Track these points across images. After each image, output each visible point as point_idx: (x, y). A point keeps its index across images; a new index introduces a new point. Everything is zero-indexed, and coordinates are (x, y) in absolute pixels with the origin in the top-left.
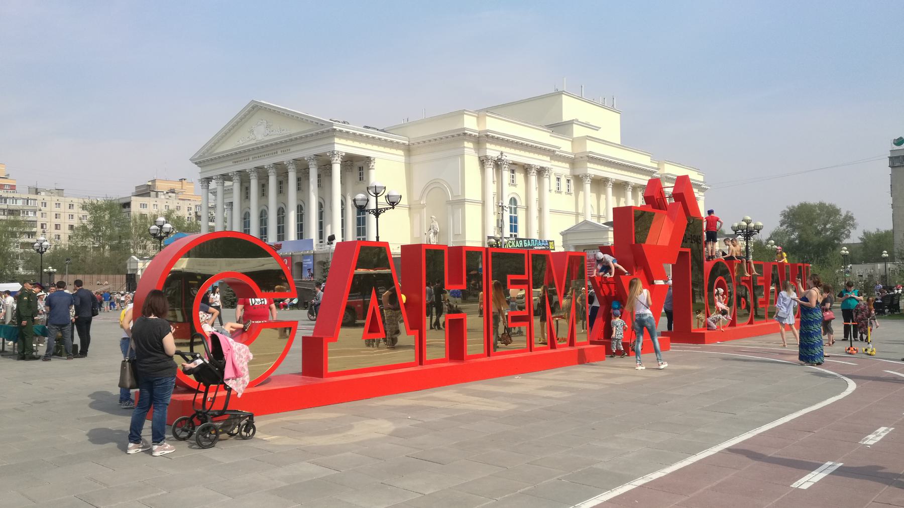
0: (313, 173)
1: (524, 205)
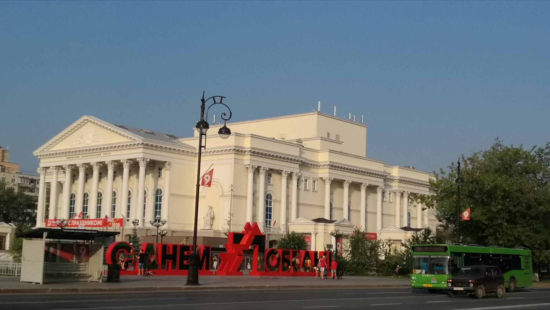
0: (96, 173)
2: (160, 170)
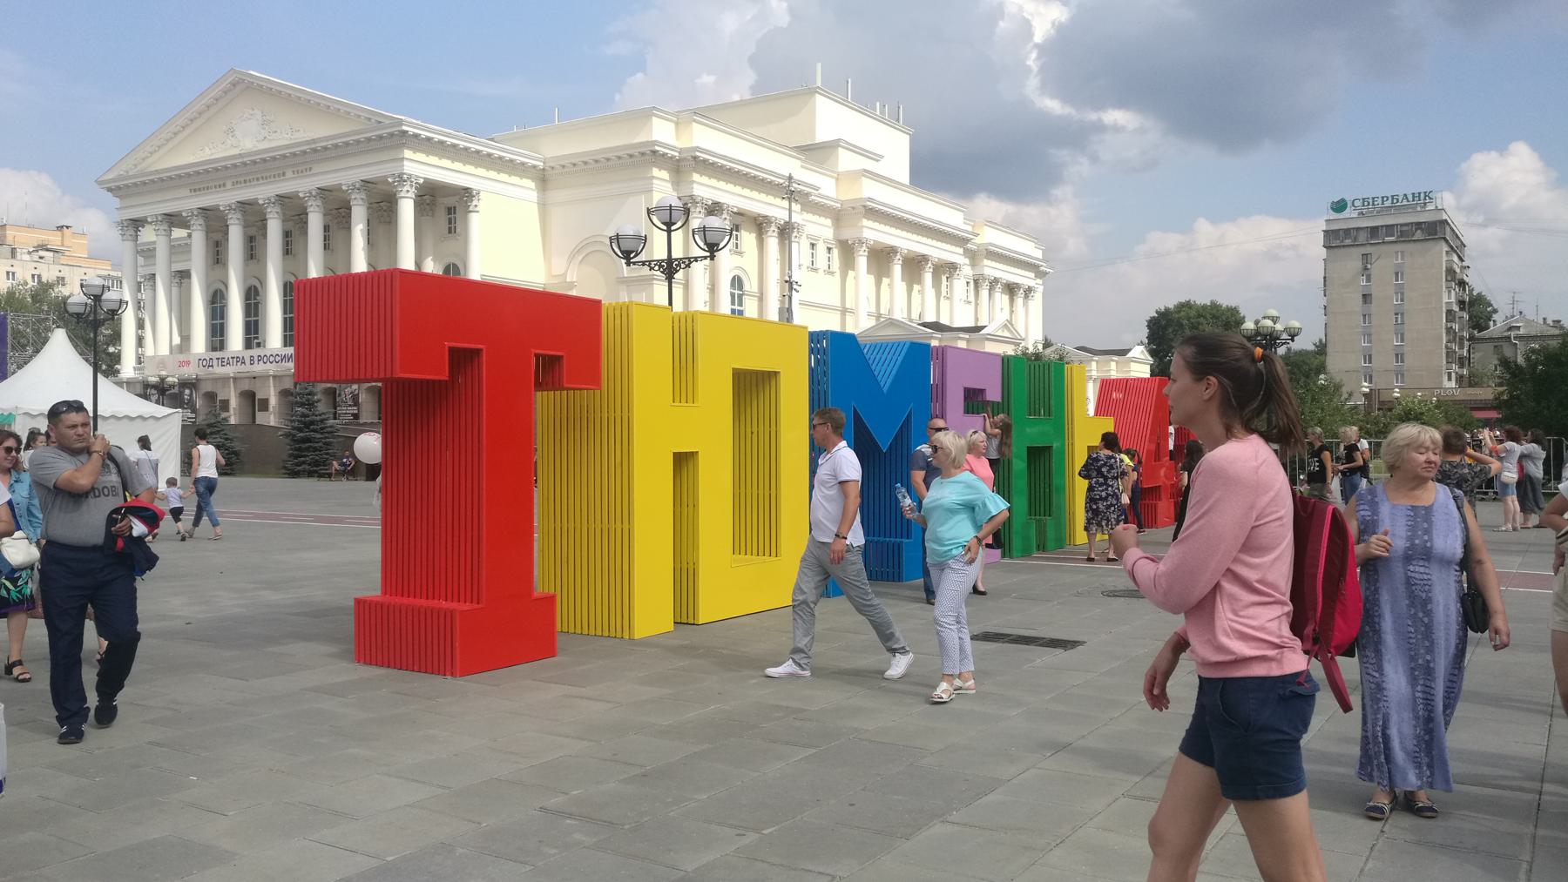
0: (315, 222)
1: (756, 291)
2: (449, 213)
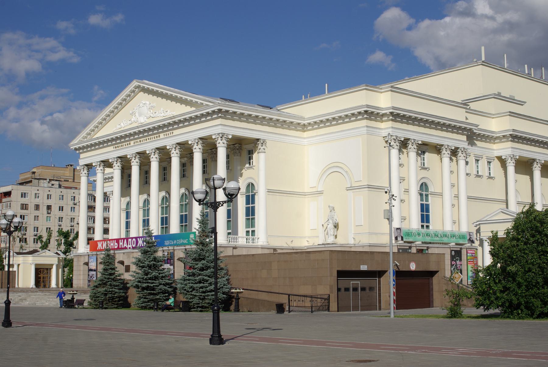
2: (249, 154)
